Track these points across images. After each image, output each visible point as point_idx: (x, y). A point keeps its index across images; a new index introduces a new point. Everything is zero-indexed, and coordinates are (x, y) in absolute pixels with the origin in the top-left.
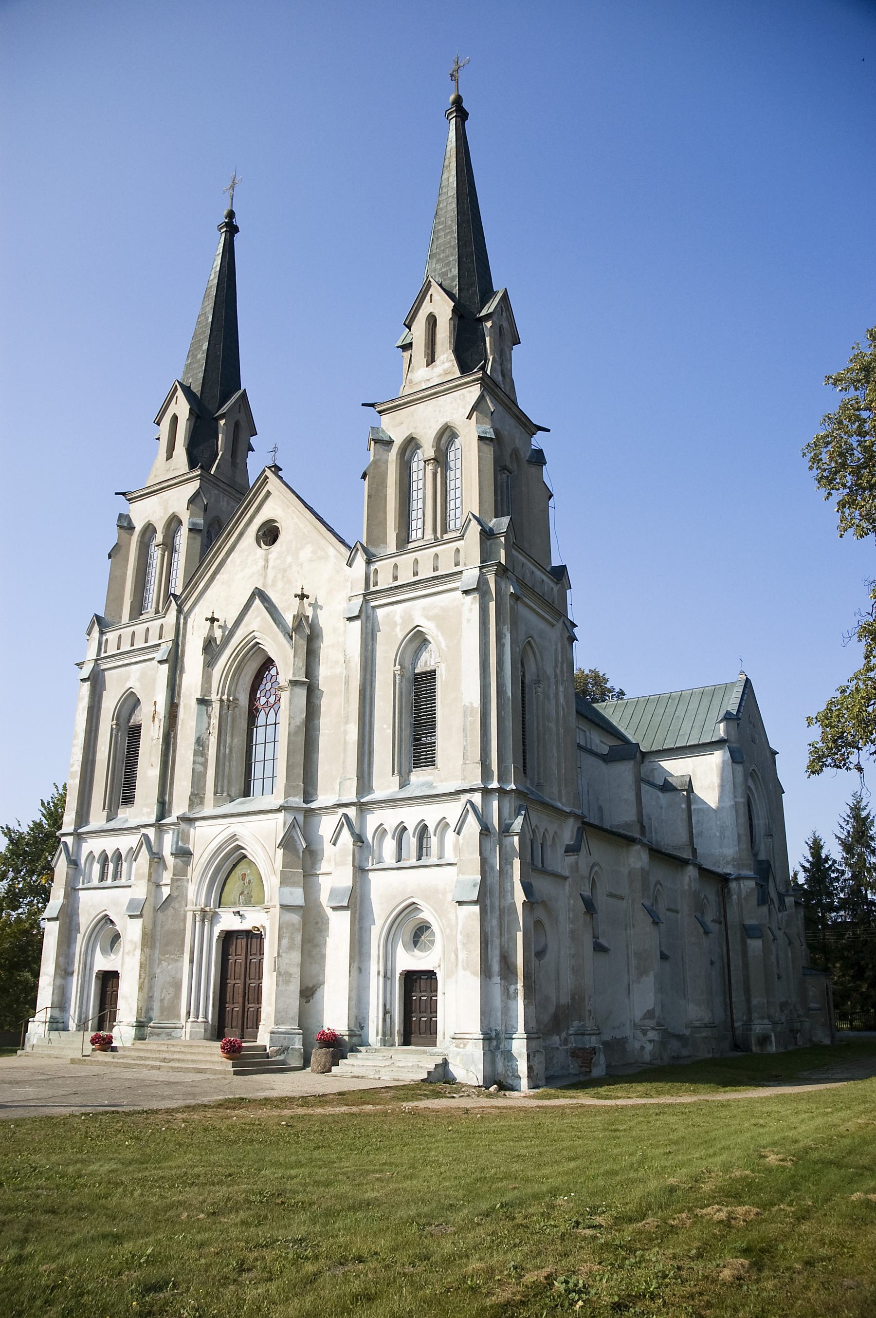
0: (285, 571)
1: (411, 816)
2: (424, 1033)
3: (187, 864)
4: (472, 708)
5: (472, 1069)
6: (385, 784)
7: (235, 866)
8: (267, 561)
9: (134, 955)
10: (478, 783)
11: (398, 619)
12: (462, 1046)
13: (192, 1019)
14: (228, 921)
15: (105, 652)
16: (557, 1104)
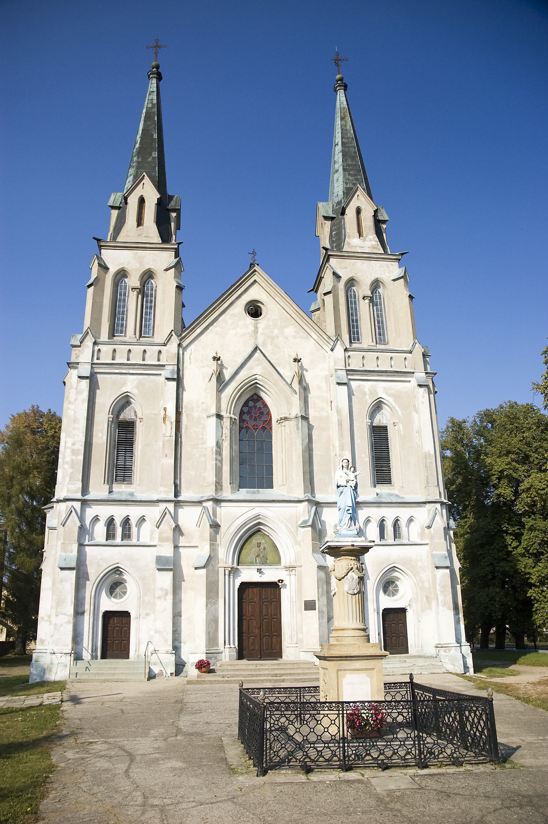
0: (273, 338)
1: (119, 513)
2: (395, 646)
3: (217, 533)
4: (430, 455)
5: (456, 664)
6: (98, 489)
7: (250, 537)
8: (256, 328)
9: (165, 599)
10: (171, 496)
11: (366, 390)
12: (448, 651)
13: (227, 646)
14: (249, 574)
15: (98, 359)
16: (254, 684)
